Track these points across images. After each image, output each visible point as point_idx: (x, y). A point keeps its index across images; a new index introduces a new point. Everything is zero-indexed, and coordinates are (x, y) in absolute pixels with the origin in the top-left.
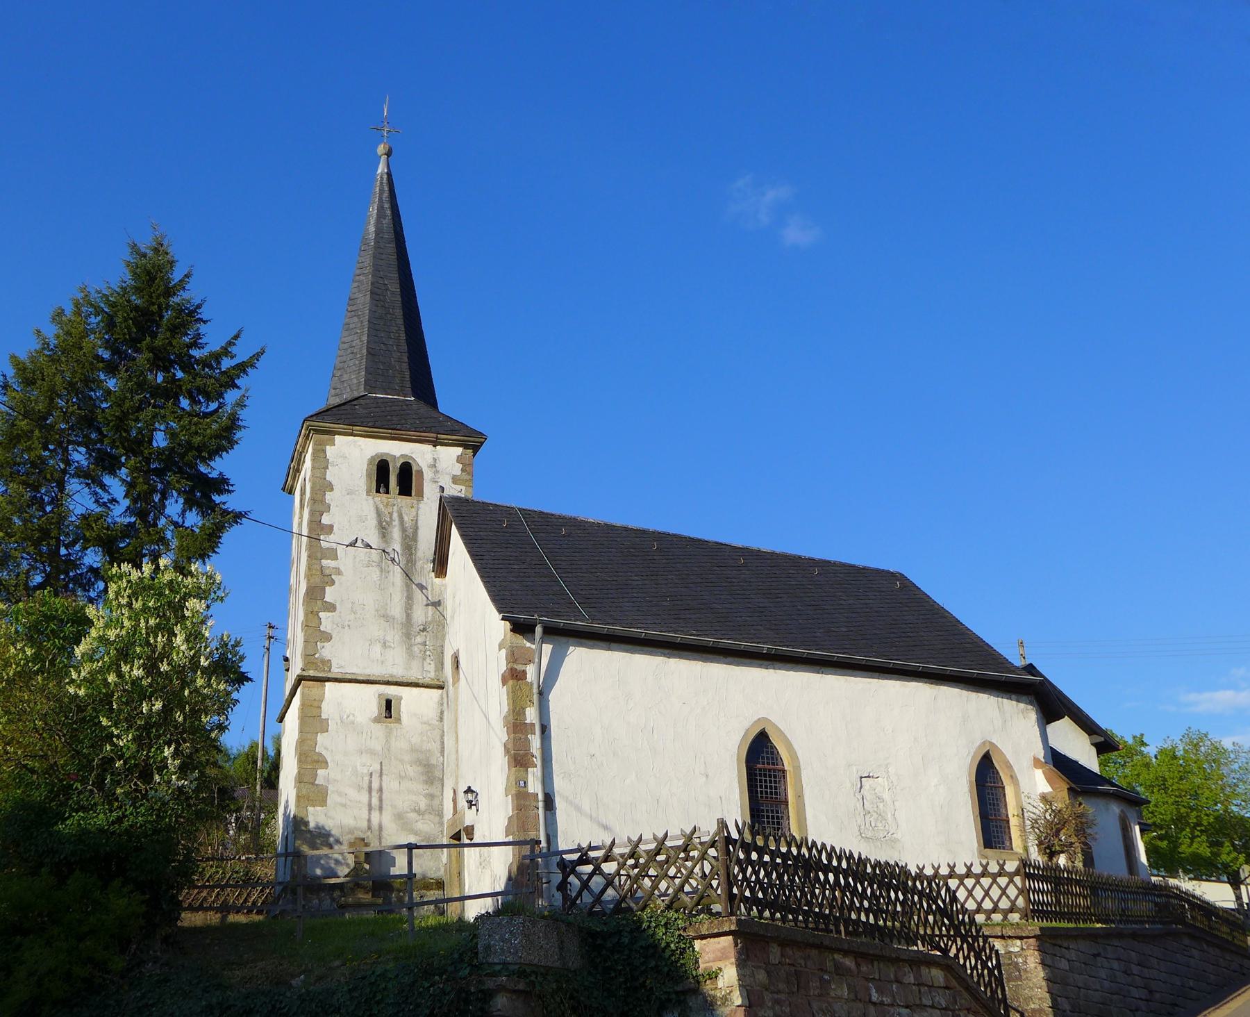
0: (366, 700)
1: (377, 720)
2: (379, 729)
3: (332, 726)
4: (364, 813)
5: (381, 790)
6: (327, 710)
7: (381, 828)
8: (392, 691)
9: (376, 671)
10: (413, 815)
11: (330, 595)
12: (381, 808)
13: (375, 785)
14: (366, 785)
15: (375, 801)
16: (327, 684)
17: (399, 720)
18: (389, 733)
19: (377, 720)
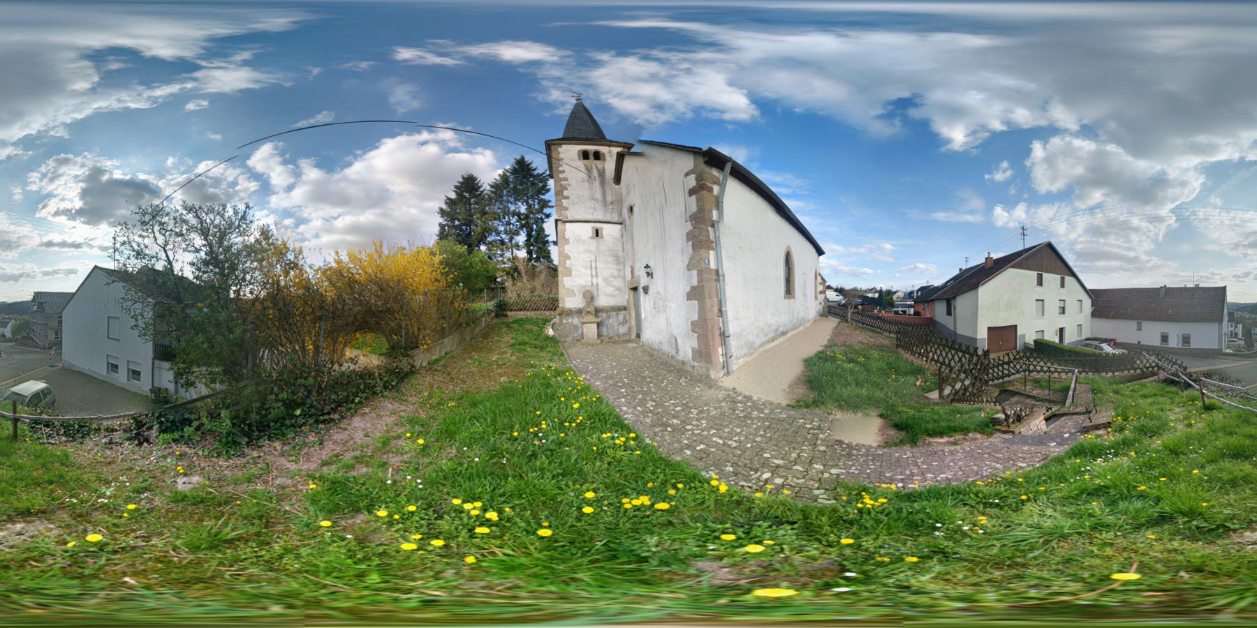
0: (587, 230)
1: (592, 238)
2: (594, 242)
3: (571, 241)
4: (590, 279)
5: (596, 268)
6: (568, 235)
7: (597, 285)
8: (598, 225)
9: (590, 217)
10: (612, 279)
11: (565, 193)
12: (597, 276)
13: (594, 266)
14: (589, 266)
15: (594, 273)
16: (567, 224)
17: (602, 237)
18: (598, 244)
19: (592, 238)
